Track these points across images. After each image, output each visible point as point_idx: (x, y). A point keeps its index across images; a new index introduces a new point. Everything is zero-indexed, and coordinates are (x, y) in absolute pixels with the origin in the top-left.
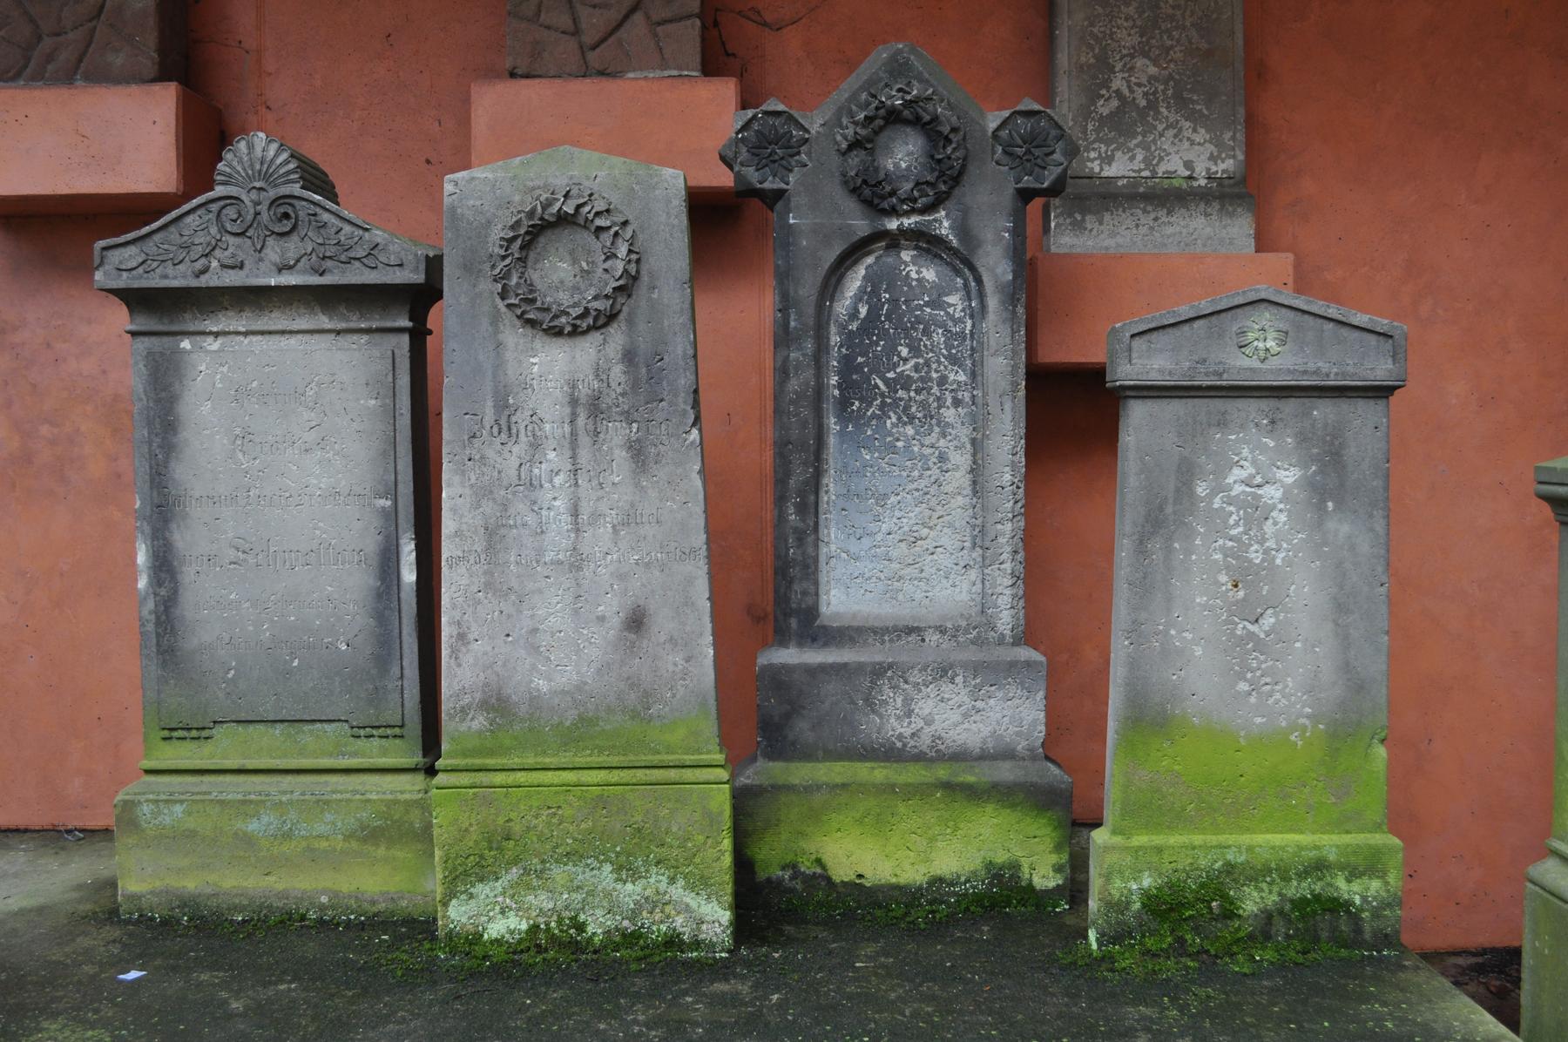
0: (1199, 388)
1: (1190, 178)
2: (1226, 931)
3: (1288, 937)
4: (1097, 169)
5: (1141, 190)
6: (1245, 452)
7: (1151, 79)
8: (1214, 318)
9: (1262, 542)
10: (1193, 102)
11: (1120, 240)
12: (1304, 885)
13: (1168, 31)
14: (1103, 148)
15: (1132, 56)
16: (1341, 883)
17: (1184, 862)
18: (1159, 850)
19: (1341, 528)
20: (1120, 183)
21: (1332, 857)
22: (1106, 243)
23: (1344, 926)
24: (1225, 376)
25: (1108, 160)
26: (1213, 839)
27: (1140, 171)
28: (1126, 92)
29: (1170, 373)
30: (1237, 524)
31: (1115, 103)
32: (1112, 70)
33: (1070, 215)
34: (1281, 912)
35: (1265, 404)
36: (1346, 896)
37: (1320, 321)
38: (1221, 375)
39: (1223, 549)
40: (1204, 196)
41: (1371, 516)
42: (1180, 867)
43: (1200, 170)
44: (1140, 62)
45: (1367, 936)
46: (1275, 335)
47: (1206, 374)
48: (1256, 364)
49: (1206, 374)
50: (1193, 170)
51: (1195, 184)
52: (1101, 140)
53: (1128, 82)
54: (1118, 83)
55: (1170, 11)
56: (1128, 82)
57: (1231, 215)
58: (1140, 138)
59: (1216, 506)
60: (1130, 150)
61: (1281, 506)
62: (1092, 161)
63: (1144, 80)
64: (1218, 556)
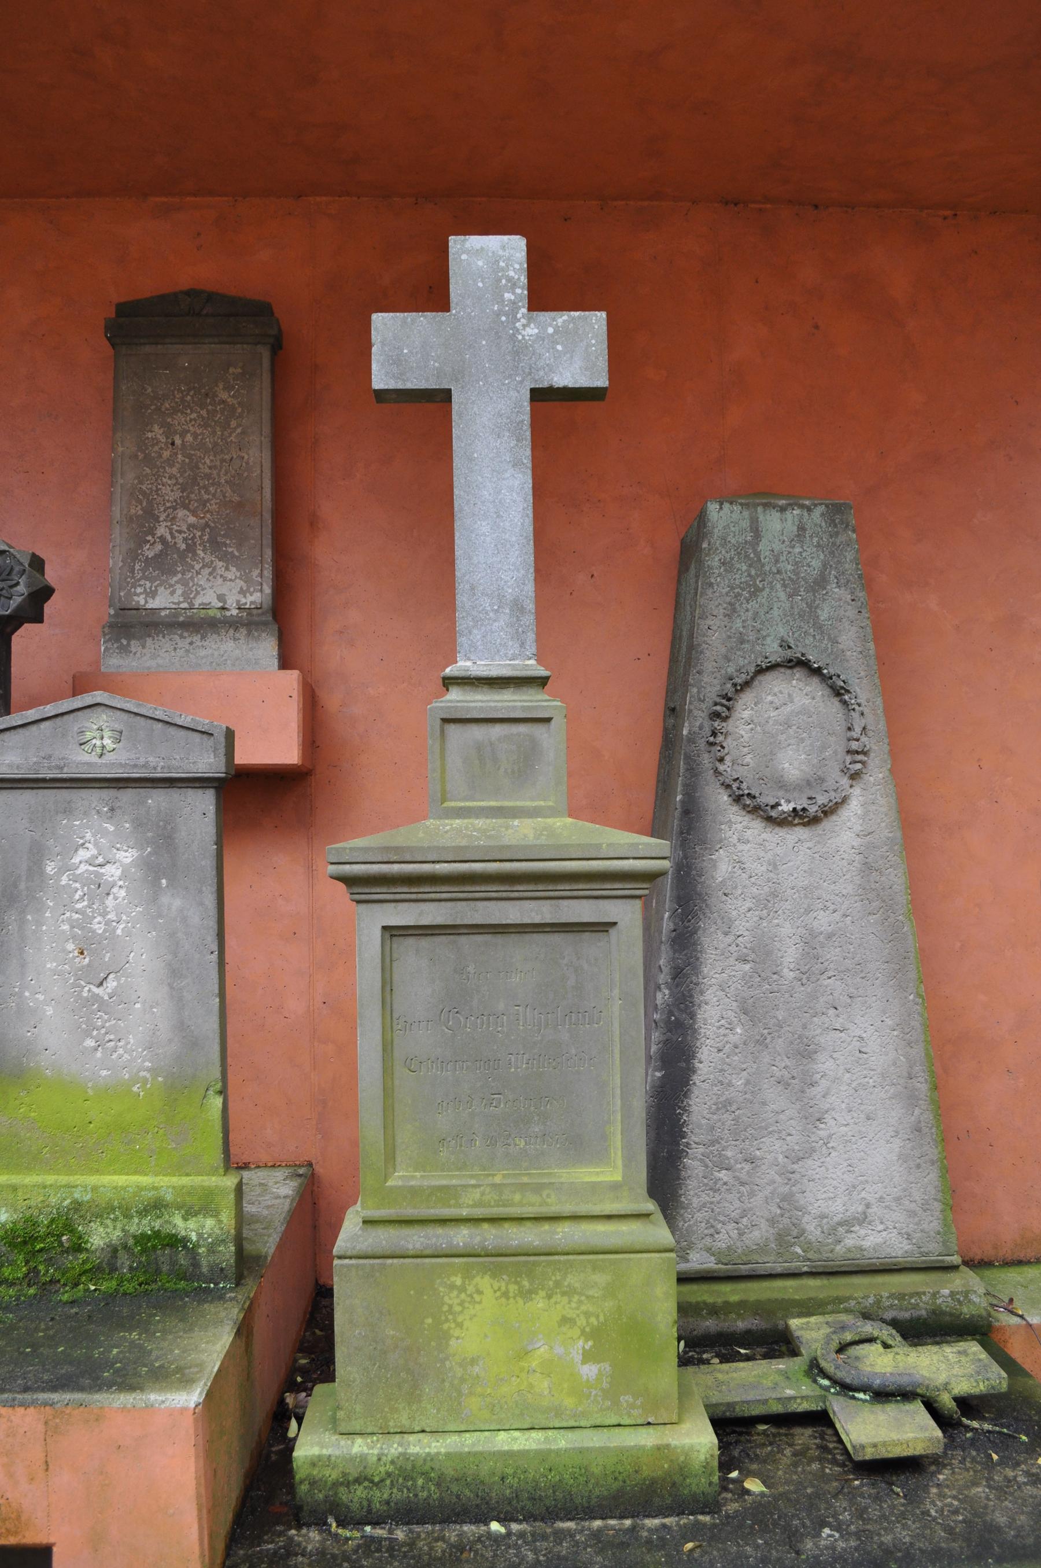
0: (44, 780)
1: (223, 608)
2: (74, 1262)
3: (131, 1268)
4: (142, 602)
5: (181, 619)
6: (88, 836)
7: (191, 527)
8: (58, 720)
9: (104, 914)
10: (226, 545)
11: (160, 661)
12: (144, 1222)
13: (204, 487)
14: (148, 584)
15: (175, 509)
16: (178, 1221)
17: (36, 1200)
18: (14, 1188)
19: (173, 902)
20: (163, 613)
21: (169, 1198)
22: (148, 664)
23: (183, 1260)
24: (65, 770)
25: (153, 594)
26: (63, 1179)
27: (179, 603)
28: (169, 538)
29: (18, 767)
30: (82, 899)
31: (159, 547)
32: (157, 520)
33: (118, 640)
34: (125, 1247)
35: (107, 794)
36: (183, 1233)
37: (150, 722)
38: (62, 768)
39: (70, 920)
40: (233, 624)
41: (200, 891)
42: (33, 1203)
43: (231, 602)
44: (181, 513)
45: (205, 1270)
46: (109, 734)
47: (49, 768)
48: (93, 758)
49: (49, 768)
50: (225, 602)
51: (228, 614)
52: (146, 578)
53: (171, 529)
54: (162, 530)
55: (207, 471)
56: (171, 529)
57: (257, 639)
58: (180, 576)
59: (63, 883)
60: (171, 586)
61: (121, 883)
62: (138, 595)
63: (184, 528)
64: (66, 927)
